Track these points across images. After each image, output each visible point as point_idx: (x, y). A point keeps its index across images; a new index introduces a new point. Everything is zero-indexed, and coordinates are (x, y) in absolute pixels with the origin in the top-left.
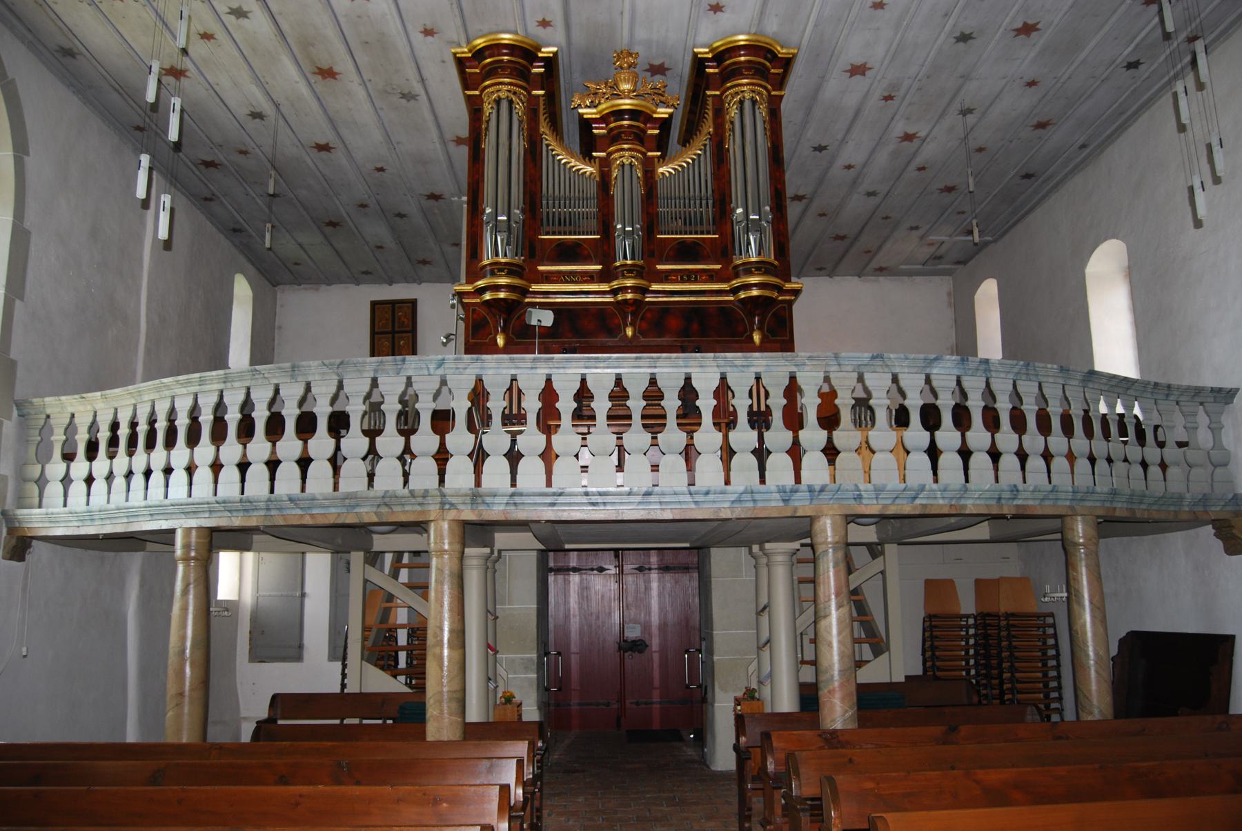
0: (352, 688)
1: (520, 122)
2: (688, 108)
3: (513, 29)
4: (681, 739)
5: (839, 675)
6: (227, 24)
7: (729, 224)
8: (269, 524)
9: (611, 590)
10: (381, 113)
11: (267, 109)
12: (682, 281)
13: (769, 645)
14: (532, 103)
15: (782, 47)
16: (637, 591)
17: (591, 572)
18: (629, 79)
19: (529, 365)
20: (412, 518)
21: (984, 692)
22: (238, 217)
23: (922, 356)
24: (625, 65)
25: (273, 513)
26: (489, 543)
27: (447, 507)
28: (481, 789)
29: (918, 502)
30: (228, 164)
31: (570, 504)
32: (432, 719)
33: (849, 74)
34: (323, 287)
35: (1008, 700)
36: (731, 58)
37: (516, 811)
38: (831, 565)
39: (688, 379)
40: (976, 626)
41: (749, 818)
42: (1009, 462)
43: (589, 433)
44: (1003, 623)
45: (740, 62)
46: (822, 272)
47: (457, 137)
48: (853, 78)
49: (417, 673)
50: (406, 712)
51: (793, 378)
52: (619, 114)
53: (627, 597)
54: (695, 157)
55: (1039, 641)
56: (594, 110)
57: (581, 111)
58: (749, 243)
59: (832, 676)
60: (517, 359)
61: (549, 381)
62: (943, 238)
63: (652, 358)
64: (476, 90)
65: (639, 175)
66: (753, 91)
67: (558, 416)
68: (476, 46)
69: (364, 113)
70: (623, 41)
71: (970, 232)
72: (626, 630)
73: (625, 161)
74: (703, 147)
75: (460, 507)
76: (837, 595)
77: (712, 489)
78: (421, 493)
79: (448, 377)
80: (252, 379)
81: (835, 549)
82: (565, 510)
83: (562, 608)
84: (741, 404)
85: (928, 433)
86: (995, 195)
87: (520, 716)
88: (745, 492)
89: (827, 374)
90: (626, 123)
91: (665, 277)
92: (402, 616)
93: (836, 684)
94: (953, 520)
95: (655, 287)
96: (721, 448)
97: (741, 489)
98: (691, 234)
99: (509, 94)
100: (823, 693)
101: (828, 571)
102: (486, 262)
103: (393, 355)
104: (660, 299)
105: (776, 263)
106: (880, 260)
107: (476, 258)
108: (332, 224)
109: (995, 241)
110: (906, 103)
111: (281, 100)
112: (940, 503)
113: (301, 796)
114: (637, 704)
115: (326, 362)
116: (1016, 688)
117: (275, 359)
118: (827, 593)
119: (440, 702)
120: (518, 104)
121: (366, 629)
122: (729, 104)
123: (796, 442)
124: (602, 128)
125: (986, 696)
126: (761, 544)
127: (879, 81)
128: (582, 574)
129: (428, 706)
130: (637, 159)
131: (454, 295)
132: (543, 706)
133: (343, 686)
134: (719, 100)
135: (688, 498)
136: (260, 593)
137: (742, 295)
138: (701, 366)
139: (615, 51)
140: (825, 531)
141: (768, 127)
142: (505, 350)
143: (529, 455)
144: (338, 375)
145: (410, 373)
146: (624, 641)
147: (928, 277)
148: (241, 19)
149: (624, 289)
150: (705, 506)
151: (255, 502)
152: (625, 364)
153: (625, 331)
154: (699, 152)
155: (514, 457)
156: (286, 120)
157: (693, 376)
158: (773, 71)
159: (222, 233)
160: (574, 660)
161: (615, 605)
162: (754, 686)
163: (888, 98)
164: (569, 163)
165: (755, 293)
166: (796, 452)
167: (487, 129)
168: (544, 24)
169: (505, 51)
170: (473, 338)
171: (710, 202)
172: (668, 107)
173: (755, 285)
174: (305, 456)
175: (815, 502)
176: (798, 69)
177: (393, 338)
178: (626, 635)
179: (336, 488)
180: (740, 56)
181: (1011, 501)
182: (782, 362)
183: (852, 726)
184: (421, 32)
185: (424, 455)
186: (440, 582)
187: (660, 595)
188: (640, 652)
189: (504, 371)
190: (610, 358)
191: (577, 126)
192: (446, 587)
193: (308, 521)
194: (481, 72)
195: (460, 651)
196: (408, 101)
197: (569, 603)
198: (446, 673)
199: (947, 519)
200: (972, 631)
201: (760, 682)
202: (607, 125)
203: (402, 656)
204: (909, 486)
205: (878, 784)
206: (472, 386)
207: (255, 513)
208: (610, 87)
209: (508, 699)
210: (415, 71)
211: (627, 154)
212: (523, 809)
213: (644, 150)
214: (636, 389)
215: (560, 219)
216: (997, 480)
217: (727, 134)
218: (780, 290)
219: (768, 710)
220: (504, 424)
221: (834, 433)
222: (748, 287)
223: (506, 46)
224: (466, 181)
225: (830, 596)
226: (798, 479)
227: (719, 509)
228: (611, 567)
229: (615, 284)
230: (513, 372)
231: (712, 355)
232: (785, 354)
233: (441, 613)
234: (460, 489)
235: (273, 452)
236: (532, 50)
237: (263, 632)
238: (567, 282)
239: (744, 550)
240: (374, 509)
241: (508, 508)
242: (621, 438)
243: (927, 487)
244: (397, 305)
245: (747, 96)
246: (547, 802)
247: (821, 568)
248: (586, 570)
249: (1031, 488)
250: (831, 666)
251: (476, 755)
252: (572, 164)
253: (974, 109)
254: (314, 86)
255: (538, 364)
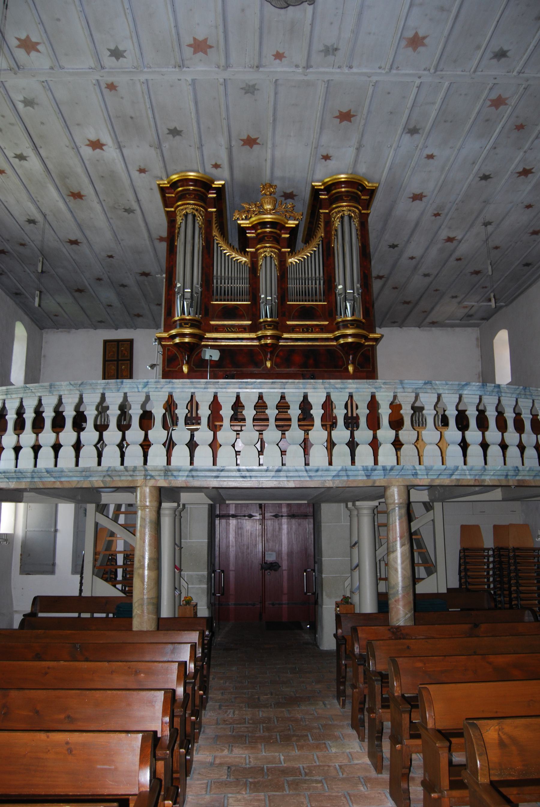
0: (86, 593)
1: (200, 228)
2: (308, 220)
4: (301, 628)
5: (402, 590)
6: (12, 163)
8: (33, 487)
9: (257, 530)
10: (111, 221)
11: (38, 217)
12: (303, 332)
13: (358, 568)
14: (208, 217)
15: (369, 182)
16: (274, 530)
17: (244, 518)
18: (270, 202)
19: (203, 386)
20: (126, 485)
21: (499, 599)
22: (19, 285)
23: (457, 383)
24: (268, 193)
25: (36, 480)
26: (176, 499)
27: (149, 477)
28: (166, 665)
29: (454, 477)
30: (13, 252)
31: (228, 477)
32: (136, 616)
33: (412, 200)
34: (74, 331)
35: (515, 605)
36: (336, 189)
37: (190, 679)
38: (397, 518)
39: (305, 397)
40: (494, 556)
41: (344, 683)
42: (513, 451)
43: (241, 430)
44: (511, 554)
45: (342, 192)
46: (396, 324)
47: (160, 237)
48: (414, 202)
49: (128, 581)
50: (121, 609)
51: (373, 397)
52: (264, 224)
53: (267, 534)
54: (312, 252)
55: (535, 566)
56: (248, 222)
57: (239, 222)
58: (346, 308)
59: (398, 590)
61: (215, 397)
62: (473, 304)
63: (282, 383)
64: (172, 207)
65: (276, 263)
66: (350, 211)
67: (221, 419)
68: (172, 180)
69: (100, 221)
70: (266, 177)
71: (490, 300)
72: (266, 556)
73: (267, 254)
74: (317, 246)
75: (157, 478)
76: (401, 537)
77: (321, 468)
78: (132, 469)
79: (151, 394)
80: (24, 393)
81: (400, 508)
82: (225, 481)
83: (225, 540)
84: (340, 413)
85: (461, 433)
86: (506, 277)
87: (196, 613)
88: (342, 470)
89: (396, 394)
90: (268, 230)
91: (292, 329)
92: (120, 546)
93: (400, 596)
94: (477, 489)
95: (285, 336)
96: (327, 441)
97: (339, 468)
98: (309, 301)
99: (193, 211)
100: (391, 601)
101: (395, 522)
102: (177, 318)
103: (117, 378)
104: (289, 344)
105: (364, 321)
106: (433, 317)
108: (79, 291)
109: (506, 306)
110: (449, 217)
111: (47, 212)
112: (468, 478)
113: (49, 668)
114: (273, 604)
115: (72, 383)
116: (520, 597)
117: (41, 380)
118: (395, 537)
119: (142, 605)
120: (199, 217)
121: (96, 553)
122: (334, 219)
123: (375, 437)
124: (253, 233)
125: (500, 602)
126: (354, 503)
127: (431, 204)
128: (238, 519)
129: (134, 608)
130: (275, 253)
131: (156, 339)
132: (211, 606)
133: (81, 591)
134: (328, 217)
135: (305, 474)
136: (28, 529)
137: (342, 341)
138: (314, 388)
139: (262, 184)
140: (393, 495)
141: (359, 234)
142: (189, 376)
144: (80, 391)
145: (126, 390)
146: (265, 563)
147: (464, 328)
148: (22, 161)
149: (265, 337)
150: (316, 479)
151: (24, 473)
152: (265, 386)
153: (266, 364)
154: (315, 249)
155: (192, 445)
156: (49, 224)
157: (309, 394)
158: (363, 197)
159: (8, 295)
160: (232, 575)
161: (259, 539)
162: (348, 595)
163: (437, 215)
164: (231, 255)
165: (350, 340)
166: (375, 444)
167: (179, 233)
168: (216, 166)
170: (168, 367)
171: (322, 282)
172: (295, 220)
173: (350, 335)
174: (57, 443)
175: (387, 477)
176: (379, 197)
177: (118, 364)
178: (266, 559)
179: (77, 465)
180: (342, 188)
181: (514, 477)
182: (367, 386)
183: (410, 623)
184: (138, 171)
186: (143, 527)
187: (288, 533)
188: (275, 570)
189: (187, 390)
190: (255, 382)
191: (237, 230)
192: (147, 531)
193: (58, 485)
194: (175, 196)
195: (156, 572)
196: (129, 213)
197: (229, 538)
198: (146, 586)
199: (473, 488)
200: (491, 559)
201: (352, 592)
202: (256, 231)
203: (120, 572)
204: (448, 467)
205: (425, 664)
207: (24, 480)
208: (258, 207)
209: (188, 602)
211: (268, 250)
212: (195, 677)
213: (279, 248)
214: (272, 402)
215: (225, 291)
216: (505, 464)
217: (333, 238)
218: (367, 339)
219: (357, 611)
220: (186, 424)
221: (400, 432)
222: (345, 336)
223: (191, 180)
224: (165, 265)
225: (396, 538)
226: (376, 462)
227: (325, 481)
228: (257, 514)
229: (260, 333)
230: (193, 390)
231: (321, 381)
232: (368, 381)
233: (144, 547)
234: (157, 466)
235: (37, 440)
237: (29, 555)
239: (343, 505)
240: (101, 479)
241: (188, 479)
242: (262, 434)
243: (460, 468)
244: (120, 343)
245: (346, 213)
246: (212, 670)
247: (391, 520)
248: (241, 516)
249: (527, 469)
250: (397, 584)
251: (164, 641)
252: (233, 256)
253: (492, 222)
254: (68, 203)
255: (209, 386)
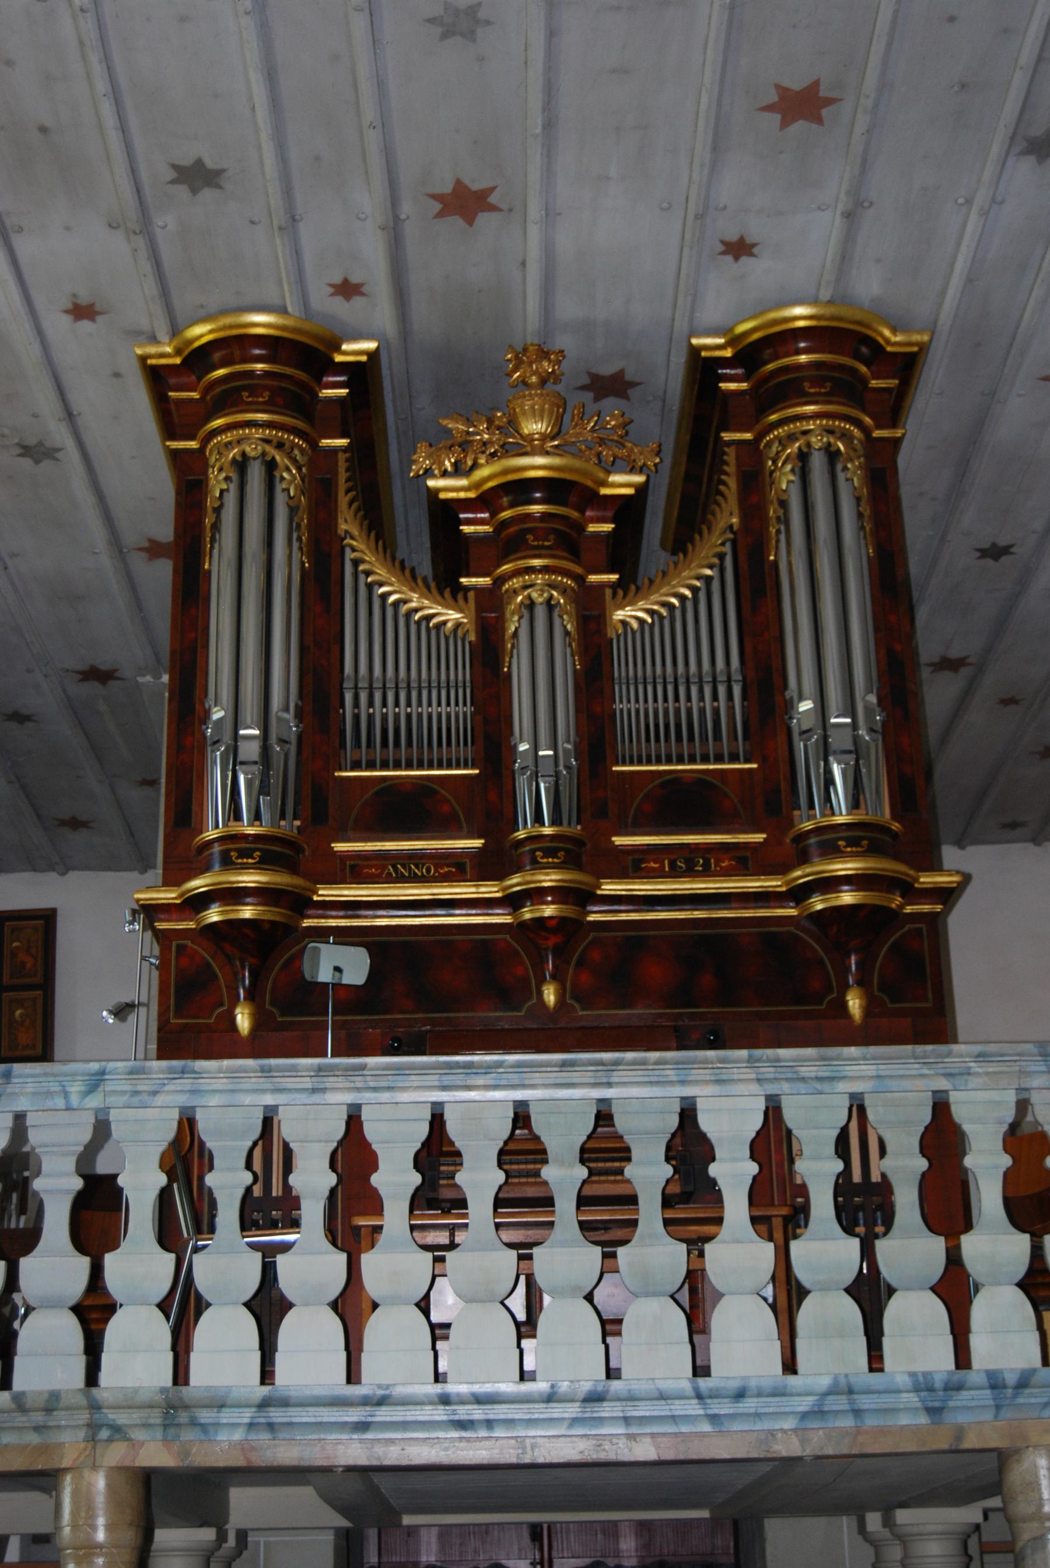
1: (293, 510)
3: (276, 301)
7: (781, 738)
12: (675, 873)
15: (894, 330)
18: (542, 410)
19: (307, 1083)
24: (534, 379)
27: (104, 1434)
31: (405, 1425)
36: (777, 357)
39: (688, 1114)
43: (452, 1246)
45: (799, 367)
54: (698, 584)
56: (463, 482)
57: (431, 483)
60: (279, 1069)
61: (354, 1121)
65: (569, 627)
66: (830, 432)
67: (374, 1204)
73: (534, 595)
74: (716, 561)
75: (138, 1435)
77: (753, 1383)
79: (114, 1115)
82: (392, 1441)
88: (833, 1391)
89: (1024, 1095)
90: (536, 509)
95: (610, 888)
96: (773, 1278)
97: (825, 1382)
102: (211, 834)
104: (623, 917)
105: (896, 826)
107: (189, 824)
120: (288, 469)
122: (775, 462)
130: (564, 591)
131: (134, 912)
134: (752, 452)
135: (693, 1408)
137: (818, 904)
138: (719, 1082)
139: (511, 348)
141: (867, 512)
143: (306, 1304)
149: (536, 895)
150: (736, 1426)
152: (537, 1078)
153: (540, 994)
157: (701, 1105)
158: (874, 383)
164: (405, 602)
165: (847, 898)
167: (216, 527)
168: (347, 289)
169: (257, 352)
170: (177, 1015)
171: (737, 690)
172: (632, 471)
173: (847, 880)
175: (1006, 1414)
182: (915, 1069)
184: (67, 312)
185: (51, 1304)
189: (248, 1099)
190: (499, 1064)
194: (203, 398)
196: (37, 462)
202: (493, 515)
206: (171, 1134)
210: (52, 396)
213: (579, 570)
217: (773, 531)
218: (910, 891)
220: (246, 1225)
222: (830, 884)
226: (962, 1357)
227: (772, 1433)
229: (515, 882)
230: (269, 1100)
231: (744, 1053)
234: (136, 1390)
236: (321, 347)
238: (401, 879)
239: (846, 1523)
241: (253, 1436)
242: (530, 1257)
245: (817, 442)
252: (413, 605)
255: (330, 1082)
